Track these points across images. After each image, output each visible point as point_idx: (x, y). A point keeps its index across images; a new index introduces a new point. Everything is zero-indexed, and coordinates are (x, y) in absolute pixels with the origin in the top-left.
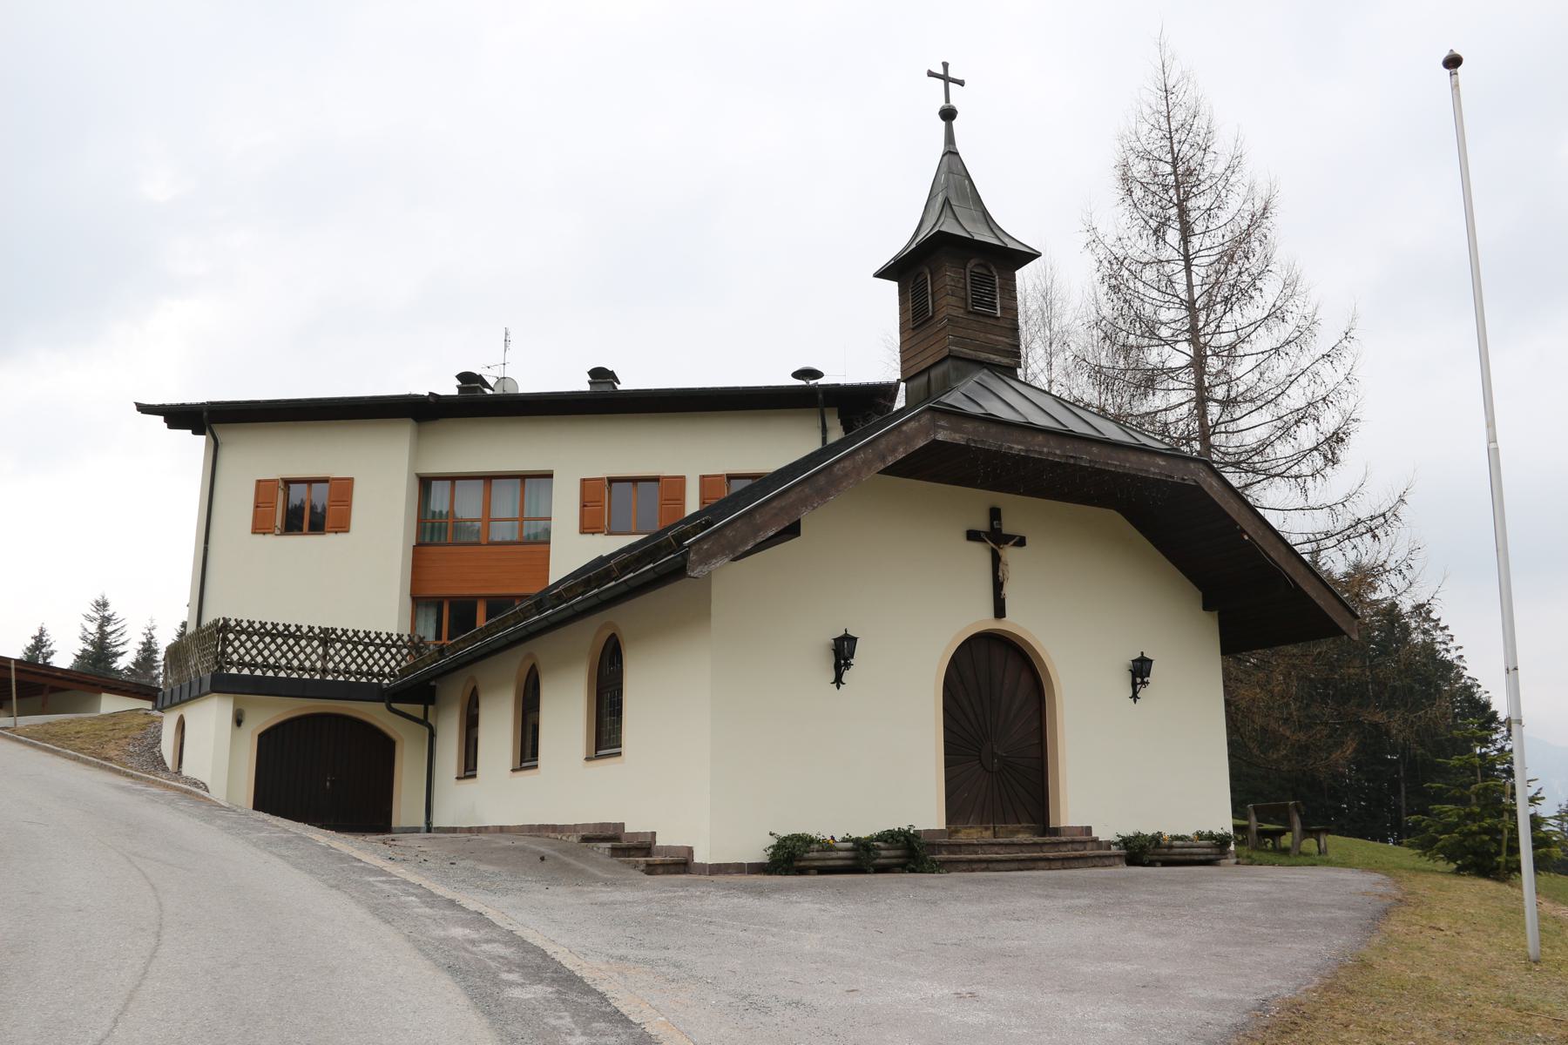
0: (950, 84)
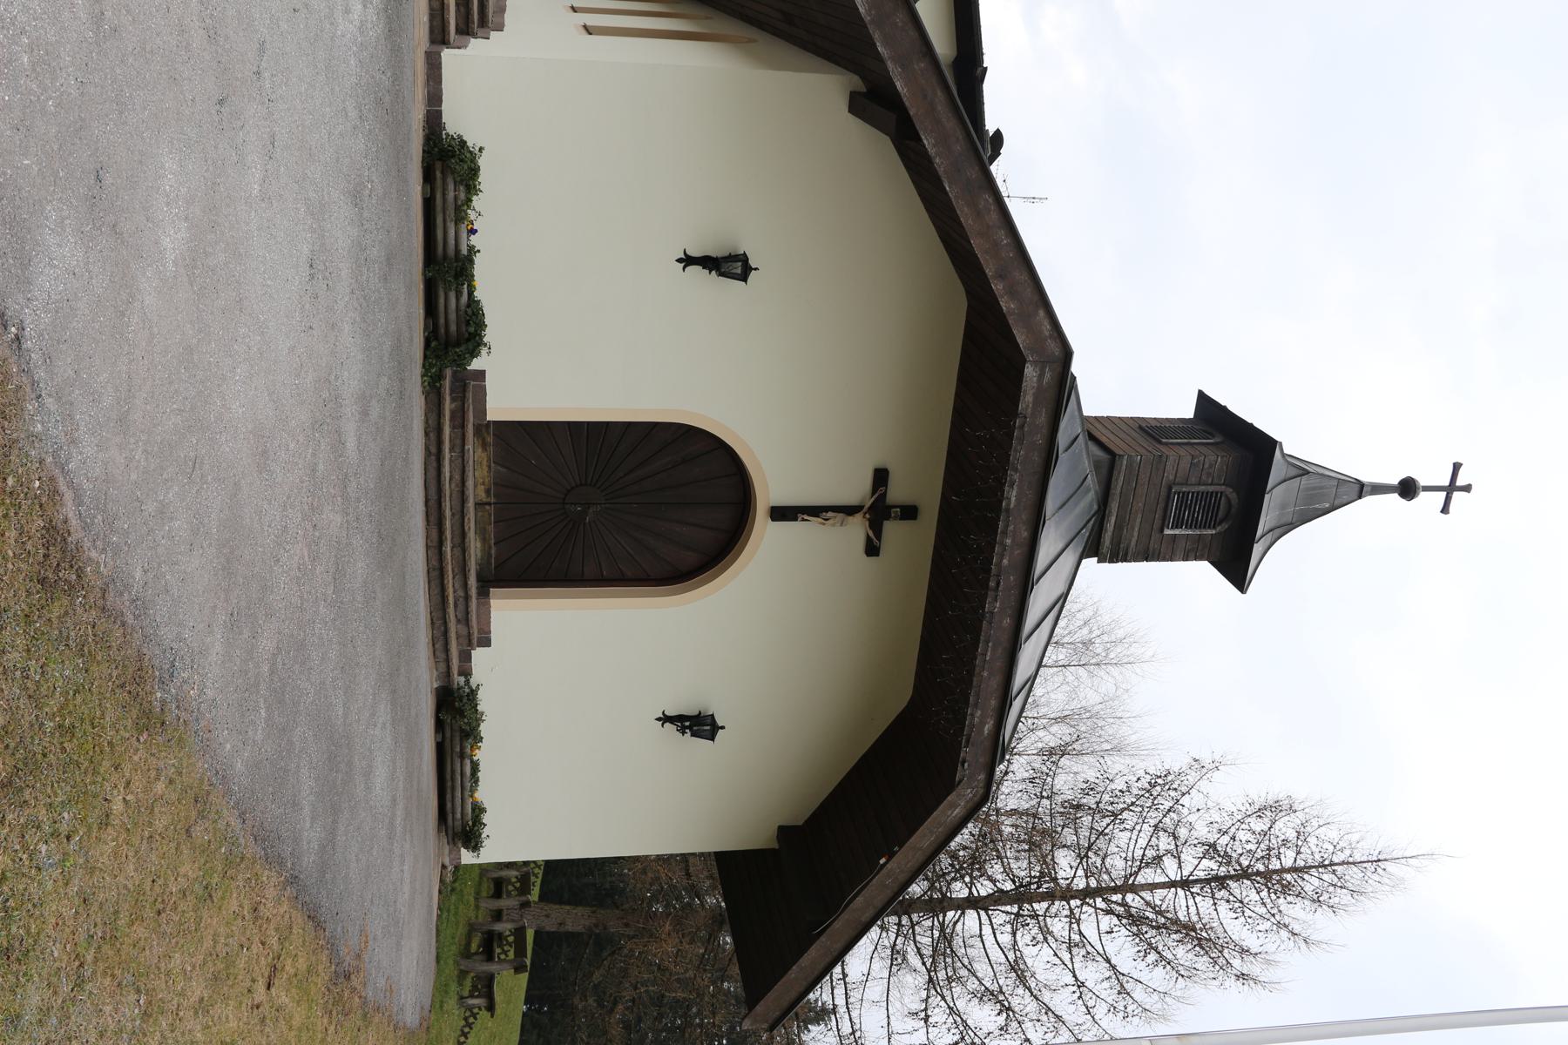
0: (1444, 494)
